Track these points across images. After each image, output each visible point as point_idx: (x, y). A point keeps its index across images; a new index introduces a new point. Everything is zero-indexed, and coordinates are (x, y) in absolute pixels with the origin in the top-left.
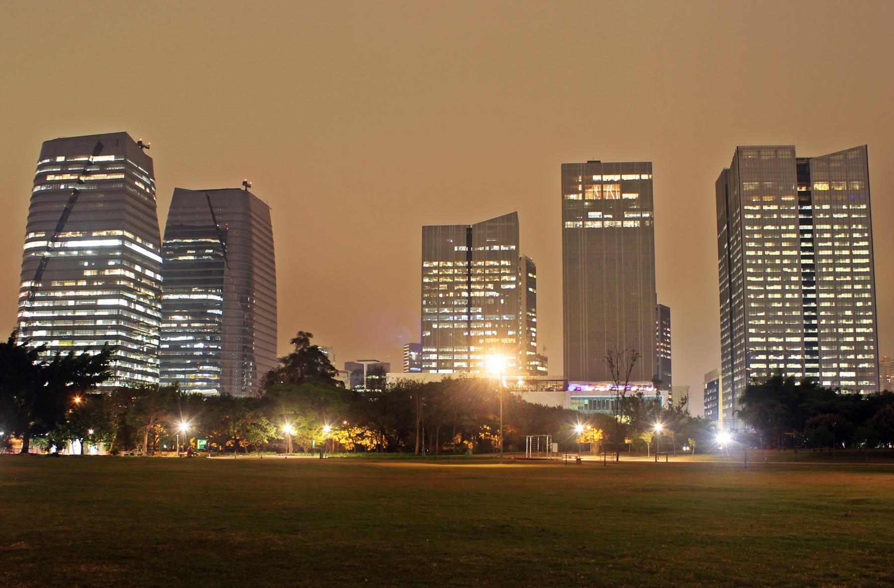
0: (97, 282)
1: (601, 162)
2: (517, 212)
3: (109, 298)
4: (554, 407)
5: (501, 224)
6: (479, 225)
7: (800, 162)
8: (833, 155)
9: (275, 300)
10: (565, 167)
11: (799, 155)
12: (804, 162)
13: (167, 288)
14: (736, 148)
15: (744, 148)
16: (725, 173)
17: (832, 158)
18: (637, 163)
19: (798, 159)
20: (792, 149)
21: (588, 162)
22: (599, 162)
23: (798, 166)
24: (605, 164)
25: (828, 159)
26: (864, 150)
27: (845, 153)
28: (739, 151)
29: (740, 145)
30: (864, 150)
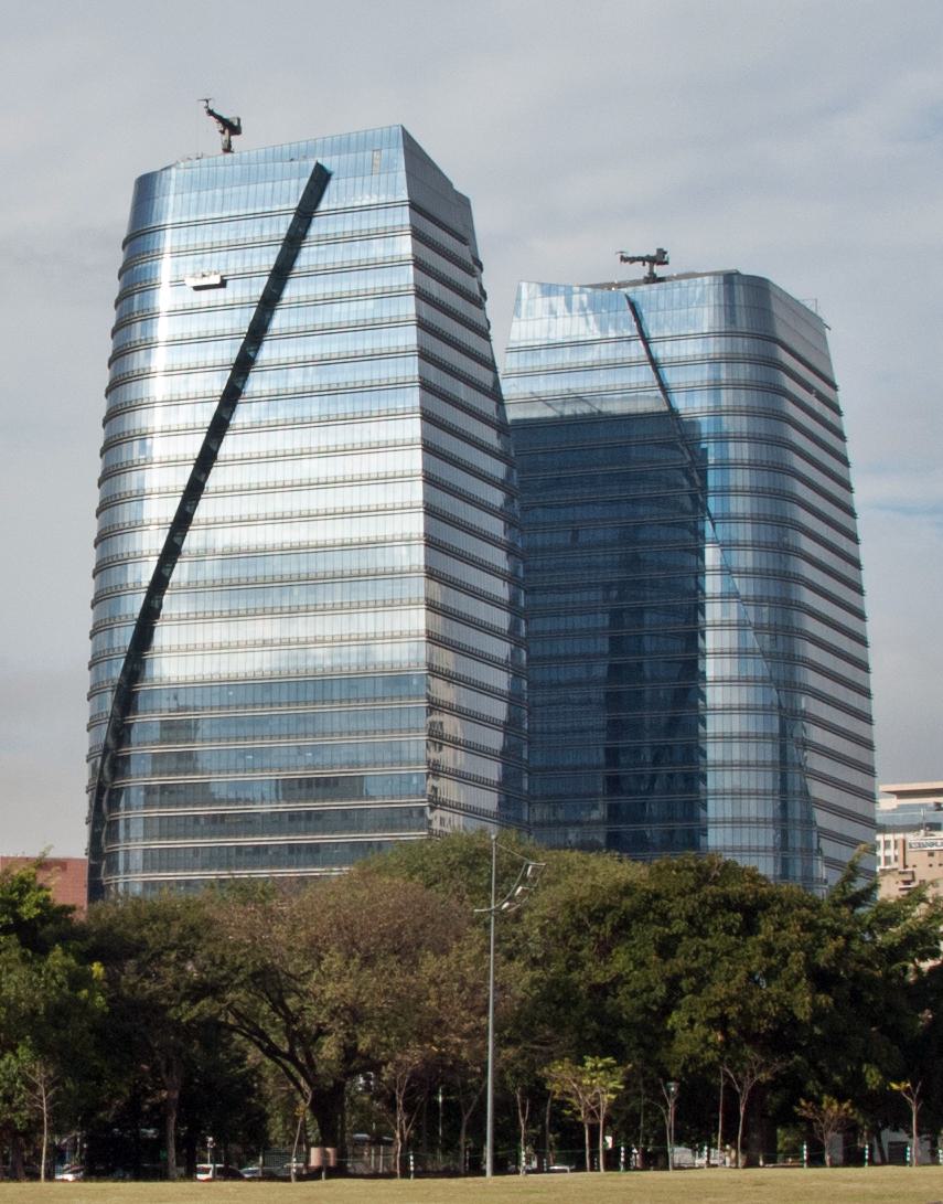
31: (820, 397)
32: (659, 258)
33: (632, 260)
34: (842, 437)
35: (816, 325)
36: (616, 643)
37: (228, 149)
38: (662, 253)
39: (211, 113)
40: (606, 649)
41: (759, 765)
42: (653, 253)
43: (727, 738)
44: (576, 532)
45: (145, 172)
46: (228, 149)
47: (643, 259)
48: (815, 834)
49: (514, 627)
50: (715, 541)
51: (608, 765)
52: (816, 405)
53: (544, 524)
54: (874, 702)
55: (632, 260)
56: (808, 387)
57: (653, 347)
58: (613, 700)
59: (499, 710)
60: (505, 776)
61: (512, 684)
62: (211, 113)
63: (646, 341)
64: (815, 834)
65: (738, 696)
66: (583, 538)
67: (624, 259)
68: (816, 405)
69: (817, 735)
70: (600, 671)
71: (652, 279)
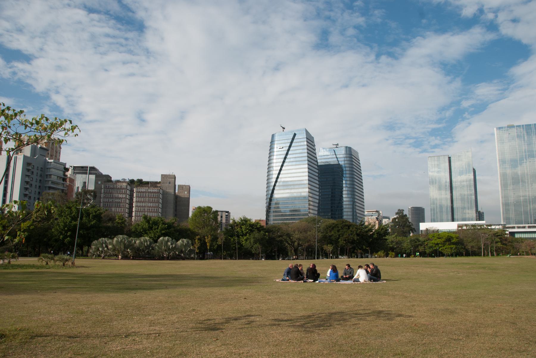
31: (358, 162)
32: (337, 145)
35: (357, 153)
52: (357, 163)
56: (356, 161)
63: (336, 155)
68: (357, 163)
70: (330, 196)
71: (337, 147)
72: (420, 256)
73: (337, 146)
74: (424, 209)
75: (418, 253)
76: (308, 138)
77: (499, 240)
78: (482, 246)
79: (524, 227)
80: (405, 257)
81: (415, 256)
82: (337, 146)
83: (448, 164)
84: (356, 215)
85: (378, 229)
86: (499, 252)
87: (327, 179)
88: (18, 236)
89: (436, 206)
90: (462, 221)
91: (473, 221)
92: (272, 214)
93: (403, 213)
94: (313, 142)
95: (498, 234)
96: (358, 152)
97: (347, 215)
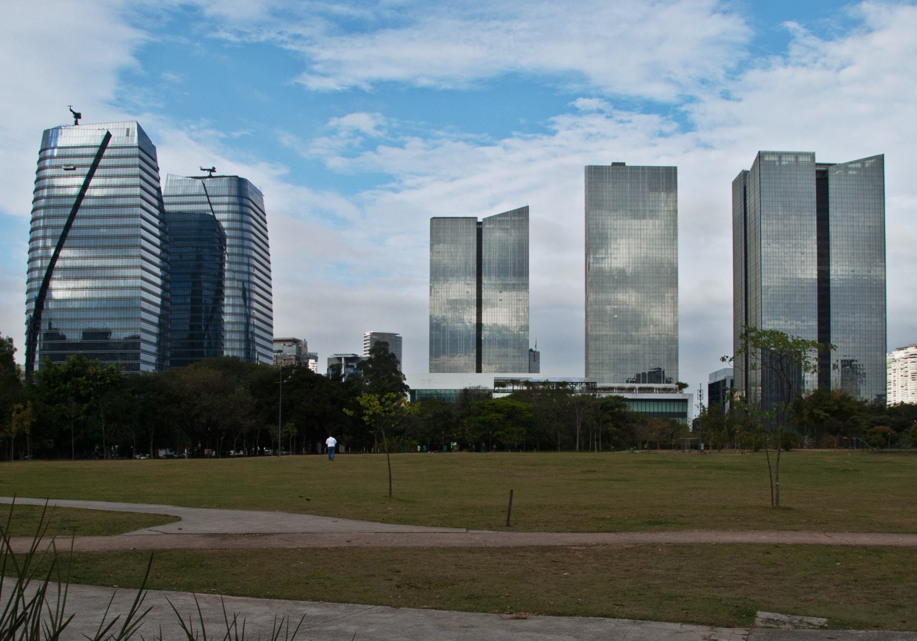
0: (589, 395)
1: (626, 165)
2: (528, 206)
3: (477, 252)
4: (279, 511)
5: (513, 218)
6: (490, 220)
7: (818, 169)
8: (851, 163)
9: (271, 326)
10: (591, 168)
11: (818, 160)
12: (823, 169)
13: (724, 399)
14: (757, 152)
15: (766, 153)
16: (744, 174)
17: (851, 166)
18: (663, 167)
19: (817, 164)
20: (813, 156)
21: (614, 164)
22: (624, 164)
23: (817, 172)
24: (632, 168)
25: (846, 167)
26: (880, 159)
27: (863, 161)
28: (760, 156)
29: (763, 149)
30: (880, 159)
31: (261, 218)
32: (213, 170)
33: (204, 170)
34: (269, 254)
35: (260, 194)
36: (194, 292)
37: (76, 123)
38: (214, 168)
39: (71, 110)
40: (191, 285)
41: (238, 297)
42: (211, 168)
43: (231, 340)
44: (181, 256)
45: (46, 129)
46: (76, 123)
47: (208, 170)
48: (256, 354)
49: (161, 244)
50: (228, 261)
51: (191, 330)
52: (260, 220)
53: (174, 253)
54: (273, 313)
55: (204, 170)
56: (258, 214)
57: (210, 198)
58: (193, 310)
59: (156, 320)
60: (158, 351)
61: (159, 321)
62: (71, 110)
63: (208, 197)
64: (256, 354)
65: (235, 336)
66: (184, 257)
67: (202, 169)
68: (260, 220)
69: (256, 297)
70: (189, 300)
71: (210, 177)
72: (461, 450)
73: (213, 174)
74: (400, 338)
75: (455, 444)
76: (143, 147)
77: (610, 418)
78: (578, 430)
79: (650, 390)
80: (422, 451)
81: (449, 450)
82: (213, 174)
83: (476, 237)
84: (254, 350)
85: (404, 384)
86: (608, 442)
87: (181, 256)
88: (834, 369)
89: (444, 336)
90: (514, 372)
91: (522, 372)
92: (898, 355)
93: (386, 352)
94: (155, 160)
95: (609, 405)
96: (262, 191)
97: (232, 348)
